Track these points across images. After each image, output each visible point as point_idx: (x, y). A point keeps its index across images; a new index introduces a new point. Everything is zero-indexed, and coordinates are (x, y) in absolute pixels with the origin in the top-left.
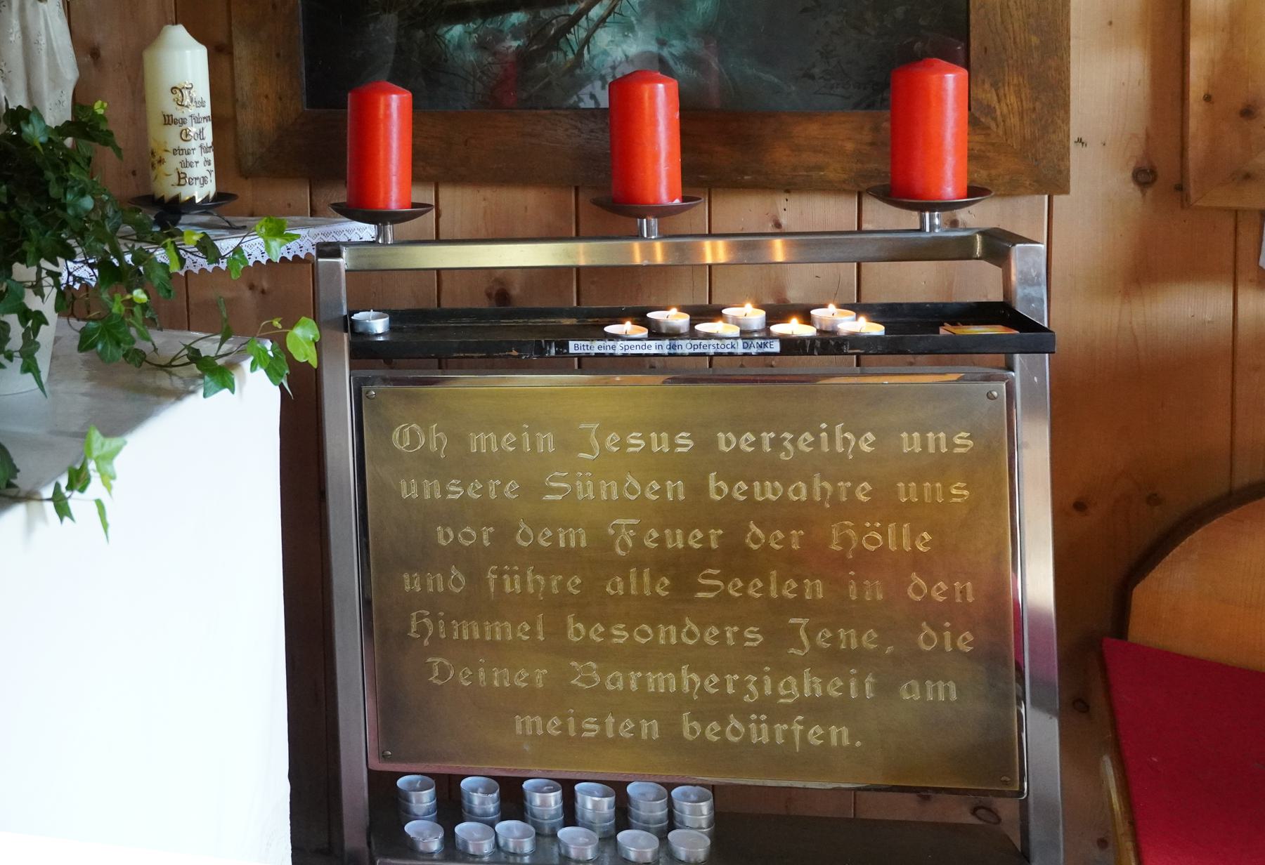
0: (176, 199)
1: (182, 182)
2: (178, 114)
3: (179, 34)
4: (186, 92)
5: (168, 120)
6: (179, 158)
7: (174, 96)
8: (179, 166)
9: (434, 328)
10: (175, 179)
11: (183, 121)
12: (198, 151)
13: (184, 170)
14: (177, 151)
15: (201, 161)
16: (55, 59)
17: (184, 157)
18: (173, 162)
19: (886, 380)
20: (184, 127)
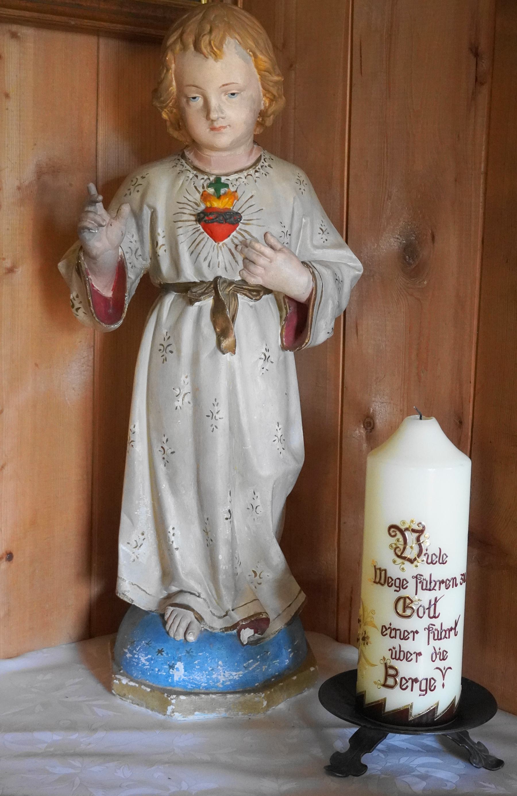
0: (381, 705)
1: (391, 681)
2: (395, 571)
3: (262, 131)
4: (411, 537)
5: (382, 578)
6: (389, 643)
7: (393, 540)
8: (388, 655)
9: (254, 22)
10: (379, 673)
11: (402, 584)
12: (423, 635)
13: (396, 664)
14: (387, 630)
15: (427, 651)
16: (242, 443)
17: (396, 642)
18: (379, 647)
19: (337, 524)
20: (403, 593)
